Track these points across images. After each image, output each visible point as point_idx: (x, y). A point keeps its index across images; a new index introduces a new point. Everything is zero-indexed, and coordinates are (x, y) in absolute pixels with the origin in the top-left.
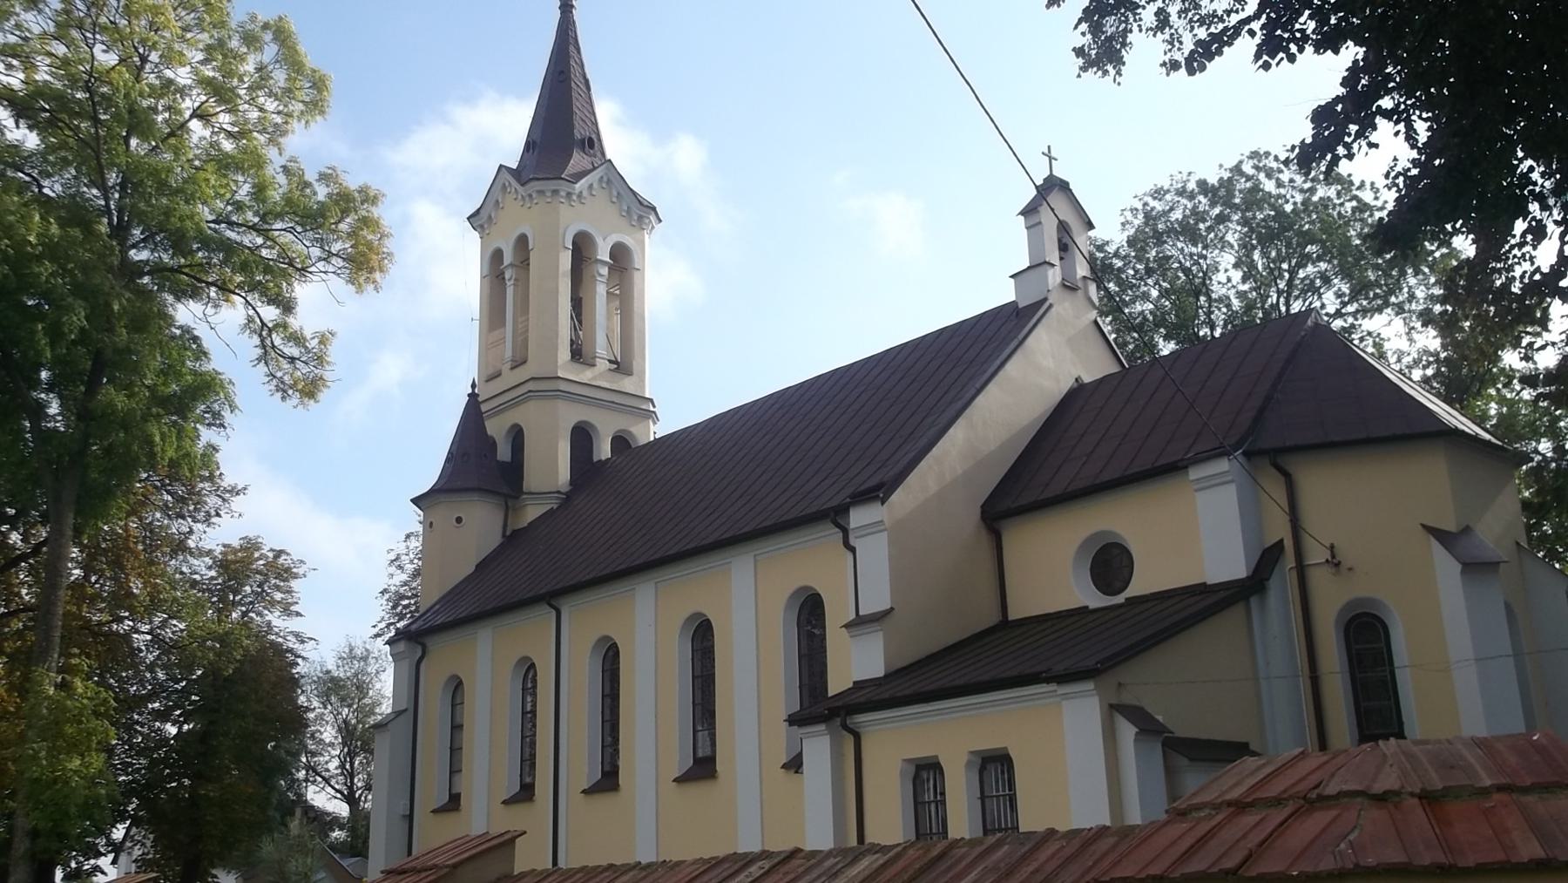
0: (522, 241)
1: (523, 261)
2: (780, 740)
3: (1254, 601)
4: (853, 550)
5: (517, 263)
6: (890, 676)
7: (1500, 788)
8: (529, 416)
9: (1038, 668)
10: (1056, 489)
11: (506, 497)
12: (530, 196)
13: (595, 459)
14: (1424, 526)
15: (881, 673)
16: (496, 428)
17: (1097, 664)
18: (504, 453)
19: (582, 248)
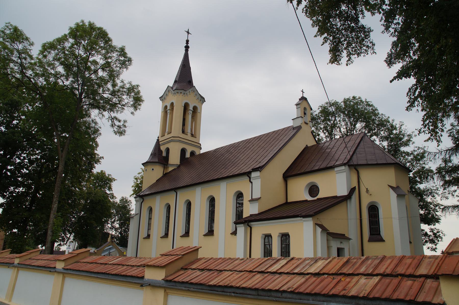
0: (172, 104)
2: (231, 227)
3: (348, 201)
4: (252, 183)
6: (259, 214)
8: (170, 146)
10: (303, 171)
11: (164, 165)
12: (175, 93)
14: (388, 185)
15: (257, 212)
16: (163, 148)
18: (164, 154)
19: (186, 106)
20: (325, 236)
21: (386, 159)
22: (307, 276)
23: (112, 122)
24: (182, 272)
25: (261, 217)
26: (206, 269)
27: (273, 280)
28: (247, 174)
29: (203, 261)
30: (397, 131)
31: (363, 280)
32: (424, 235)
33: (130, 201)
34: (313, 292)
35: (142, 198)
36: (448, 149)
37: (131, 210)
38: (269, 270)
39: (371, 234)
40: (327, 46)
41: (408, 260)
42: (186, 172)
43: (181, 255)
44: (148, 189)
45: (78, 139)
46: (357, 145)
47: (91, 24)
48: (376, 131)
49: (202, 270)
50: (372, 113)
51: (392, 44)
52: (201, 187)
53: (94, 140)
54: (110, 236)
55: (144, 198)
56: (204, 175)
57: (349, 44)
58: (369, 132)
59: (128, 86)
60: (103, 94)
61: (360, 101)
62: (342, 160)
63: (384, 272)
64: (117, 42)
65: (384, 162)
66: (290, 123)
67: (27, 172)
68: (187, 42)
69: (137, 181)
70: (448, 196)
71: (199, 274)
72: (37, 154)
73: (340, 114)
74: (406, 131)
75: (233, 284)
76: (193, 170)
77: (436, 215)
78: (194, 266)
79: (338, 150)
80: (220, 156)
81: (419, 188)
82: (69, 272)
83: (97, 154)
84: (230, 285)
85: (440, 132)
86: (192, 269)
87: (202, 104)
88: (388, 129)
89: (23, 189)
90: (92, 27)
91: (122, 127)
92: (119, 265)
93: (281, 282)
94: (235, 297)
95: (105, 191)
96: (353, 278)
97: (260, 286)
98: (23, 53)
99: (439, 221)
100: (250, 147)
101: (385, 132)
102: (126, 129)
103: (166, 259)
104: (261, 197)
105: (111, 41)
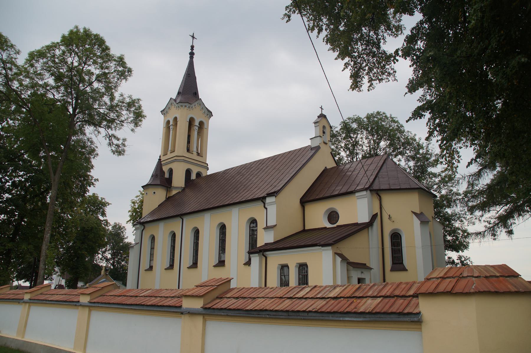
0: (175, 119)
2: (244, 258)
3: (370, 228)
4: (266, 209)
6: (275, 243)
7: (501, 276)
8: (173, 166)
9: (317, 242)
10: (321, 196)
11: (167, 187)
12: (179, 107)
13: (192, 179)
15: (272, 241)
16: (165, 169)
18: (167, 176)
19: (191, 122)
21: (409, 183)
22: (328, 300)
23: (109, 140)
24: (218, 301)
25: (277, 246)
26: (240, 297)
27: (300, 303)
29: (236, 291)
30: (424, 151)
31: (370, 301)
32: (451, 263)
33: (124, 227)
34: (332, 311)
35: (143, 225)
36: (471, 175)
37: (126, 238)
38: (297, 296)
39: (393, 263)
40: (348, 72)
41: (404, 285)
42: (192, 196)
43: (216, 285)
44: (150, 215)
45: (72, 160)
46: (379, 168)
47: (87, 31)
48: (401, 149)
49: (237, 298)
50: (397, 130)
51: (414, 70)
52: (210, 214)
53: (88, 161)
54: (104, 268)
55: (146, 225)
56: (213, 200)
57: (370, 70)
58: (393, 151)
59: (128, 100)
60: (99, 110)
61: (384, 116)
63: (385, 294)
64: (115, 52)
66: (307, 143)
67: (10, 196)
68: (192, 47)
69: (135, 205)
70: (475, 221)
71: (235, 302)
72: (20, 176)
73: (363, 131)
74: (434, 150)
75: (267, 308)
76: (200, 194)
78: (228, 295)
79: (359, 173)
80: (230, 178)
81: (447, 212)
82: (96, 305)
83: (91, 176)
84: (264, 309)
85: (456, 163)
86: (227, 298)
87: (209, 119)
89: (4, 217)
90: (87, 34)
91: (121, 146)
92: (151, 296)
93: (307, 305)
94: (269, 318)
95: (98, 217)
96: (363, 300)
97: (290, 308)
98: (8, 63)
100: (264, 169)
101: (412, 152)
102: (125, 148)
103: (202, 290)
104: (276, 225)
105: (109, 49)
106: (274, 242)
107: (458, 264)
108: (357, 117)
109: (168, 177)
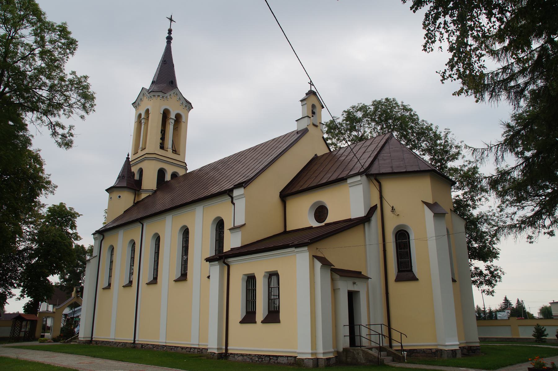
0: (147, 111)
1: (147, 118)
3: (366, 224)
4: (234, 204)
5: (146, 118)
6: (242, 247)
8: (143, 165)
10: (305, 187)
11: (135, 190)
12: (151, 97)
13: (166, 180)
14: (422, 201)
15: (240, 246)
16: (135, 169)
17: (308, 240)
19: (166, 114)
20: (328, 274)
28: (228, 192)
30: (442, 141)
32: (478, 274)
55: (105, 234)
62: (358, 168)
65: (416, 169)
66: (294, 127)
68: (170, 31)
77: (493, 248)
87: (189, 112)
88: (431, 140)
91: (68, 135)
99: (497, 256)
104: (245, 224)
106: (241, 247)
107: (487, 275)
108: (362, 105)
109: (138, 179)
